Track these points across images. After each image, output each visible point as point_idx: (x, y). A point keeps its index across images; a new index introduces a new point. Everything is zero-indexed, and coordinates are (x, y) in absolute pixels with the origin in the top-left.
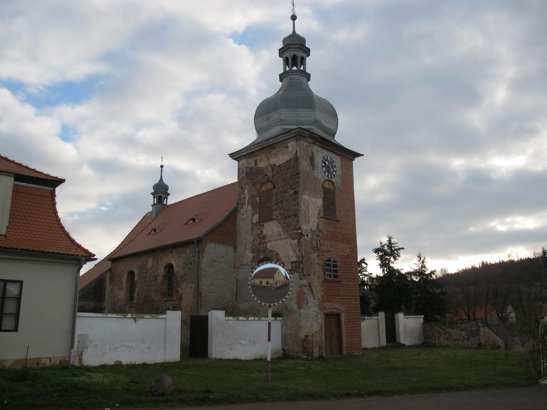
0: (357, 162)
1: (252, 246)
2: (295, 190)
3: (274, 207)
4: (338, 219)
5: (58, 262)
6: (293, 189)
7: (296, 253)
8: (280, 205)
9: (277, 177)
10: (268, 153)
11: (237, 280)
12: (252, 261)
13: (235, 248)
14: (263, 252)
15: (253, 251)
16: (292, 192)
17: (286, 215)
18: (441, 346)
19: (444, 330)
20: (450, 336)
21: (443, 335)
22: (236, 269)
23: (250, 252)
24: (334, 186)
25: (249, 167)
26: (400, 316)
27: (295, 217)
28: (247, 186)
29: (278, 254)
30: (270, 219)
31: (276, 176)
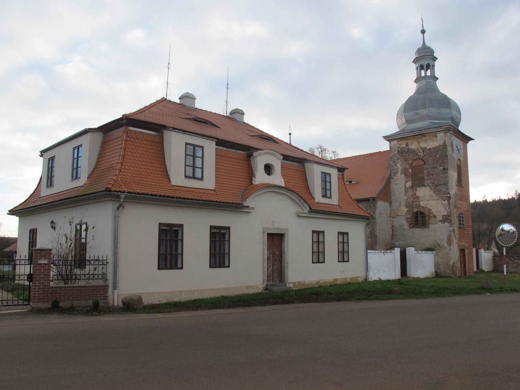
0: (470, 144)
1: (406, 202)
2: (444, 167)
3: (426, 177)
4: (463, 186)
5: (153, 204)
6: (443, 166)
7: (447, 210)
8: (431, 176)
9: (427, 157)
10: (418, 139)
11: (393, 226)
12: (406, 213)
13: (391, 204)
14: (417, 208)
15: (407, 206)
16: (441, 168)
17: (436, 184)
18: (509, 272)
19: (513, 261)
20: (518, 265)
21: (511, 265)
22: (392, 219)
23: (404, 207)
24: (461, 163)
25: (401, 147)
26: (482, 251)
27: (444, 186)
28: (399, 161)
29: (430, 209)
30: (421, 186)
31: (426, 156)
